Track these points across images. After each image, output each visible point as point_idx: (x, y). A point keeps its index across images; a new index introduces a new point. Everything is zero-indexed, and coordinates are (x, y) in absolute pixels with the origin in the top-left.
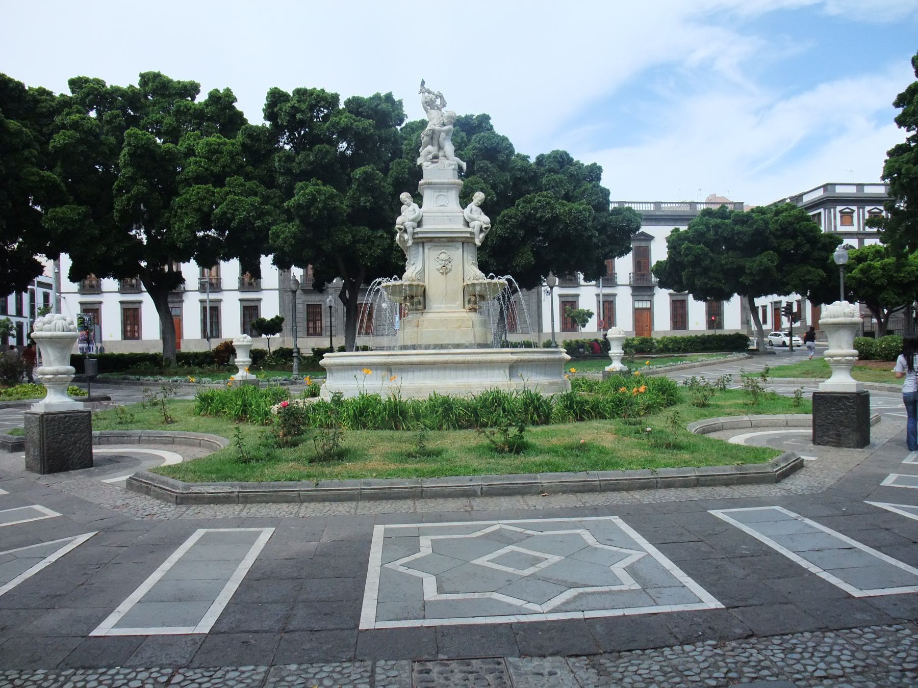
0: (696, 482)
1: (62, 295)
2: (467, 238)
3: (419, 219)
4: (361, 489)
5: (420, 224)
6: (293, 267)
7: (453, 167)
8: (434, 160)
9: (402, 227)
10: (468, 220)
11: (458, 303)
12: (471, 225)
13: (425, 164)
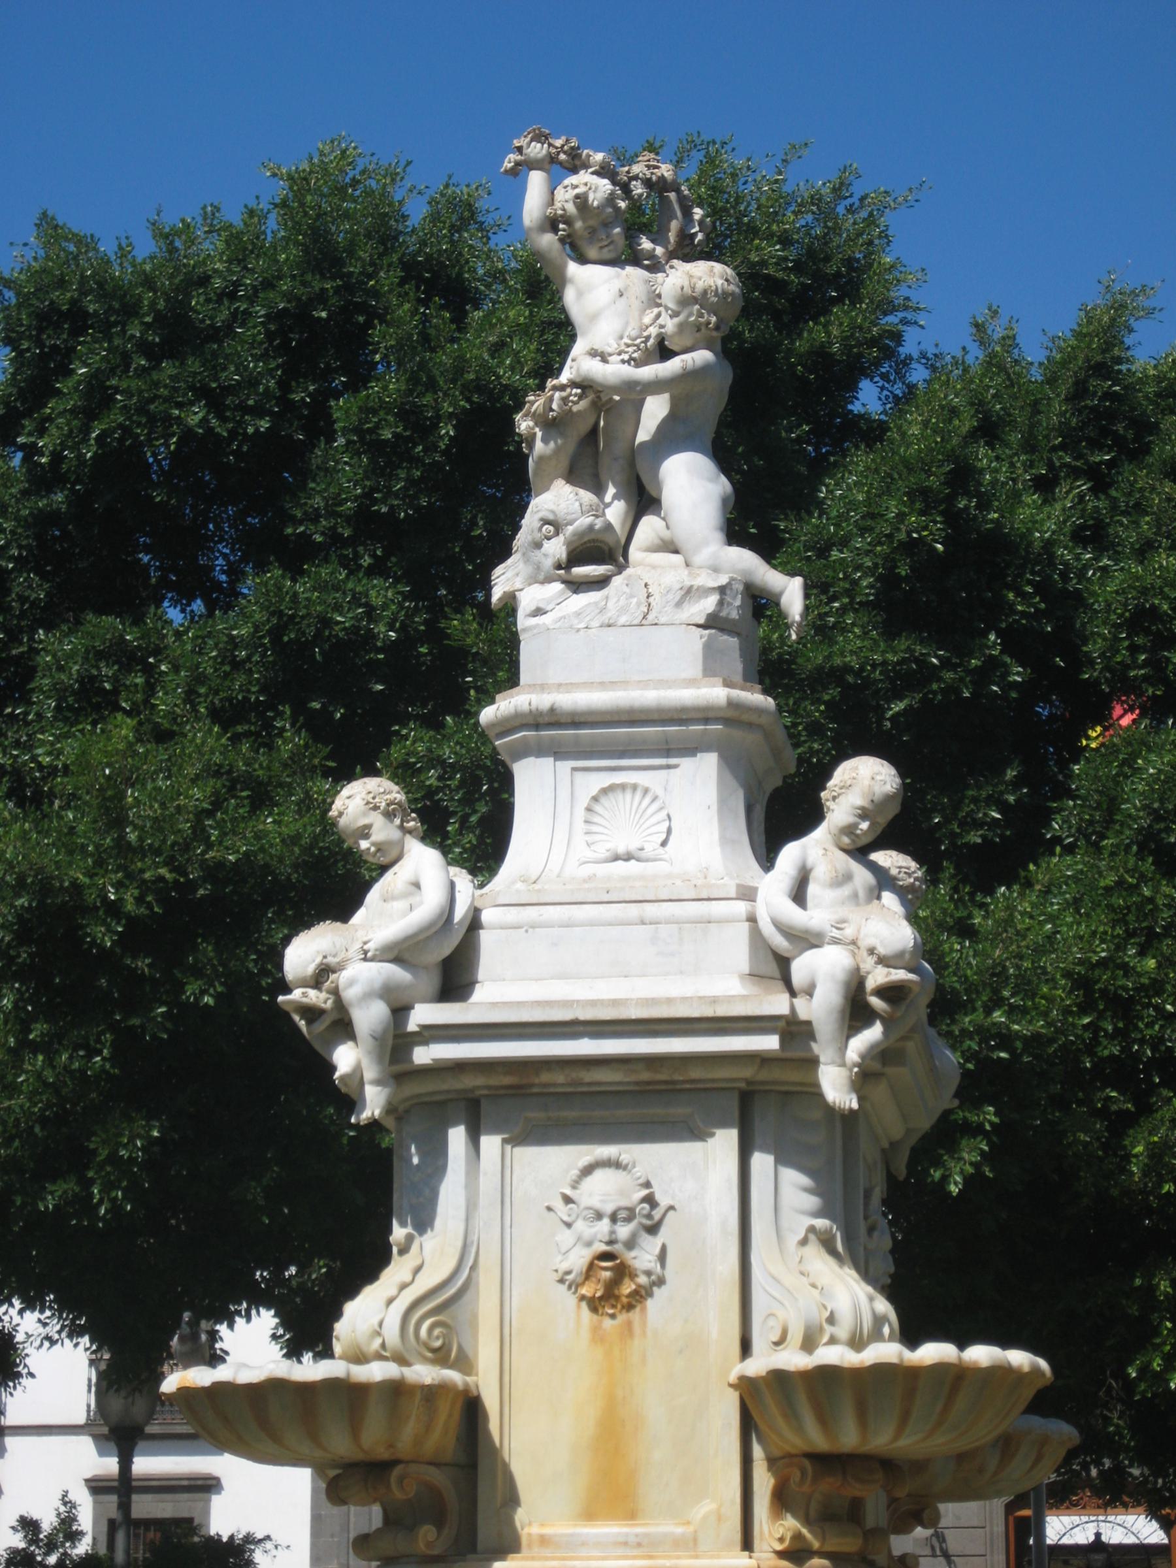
6: (1049, 1542)
7: (709, 604)
8: (580, 571)
9: (314, 997)
10: (779, 942)
11: (706, 1507)
12: (801, 968)
13: (528, 599)
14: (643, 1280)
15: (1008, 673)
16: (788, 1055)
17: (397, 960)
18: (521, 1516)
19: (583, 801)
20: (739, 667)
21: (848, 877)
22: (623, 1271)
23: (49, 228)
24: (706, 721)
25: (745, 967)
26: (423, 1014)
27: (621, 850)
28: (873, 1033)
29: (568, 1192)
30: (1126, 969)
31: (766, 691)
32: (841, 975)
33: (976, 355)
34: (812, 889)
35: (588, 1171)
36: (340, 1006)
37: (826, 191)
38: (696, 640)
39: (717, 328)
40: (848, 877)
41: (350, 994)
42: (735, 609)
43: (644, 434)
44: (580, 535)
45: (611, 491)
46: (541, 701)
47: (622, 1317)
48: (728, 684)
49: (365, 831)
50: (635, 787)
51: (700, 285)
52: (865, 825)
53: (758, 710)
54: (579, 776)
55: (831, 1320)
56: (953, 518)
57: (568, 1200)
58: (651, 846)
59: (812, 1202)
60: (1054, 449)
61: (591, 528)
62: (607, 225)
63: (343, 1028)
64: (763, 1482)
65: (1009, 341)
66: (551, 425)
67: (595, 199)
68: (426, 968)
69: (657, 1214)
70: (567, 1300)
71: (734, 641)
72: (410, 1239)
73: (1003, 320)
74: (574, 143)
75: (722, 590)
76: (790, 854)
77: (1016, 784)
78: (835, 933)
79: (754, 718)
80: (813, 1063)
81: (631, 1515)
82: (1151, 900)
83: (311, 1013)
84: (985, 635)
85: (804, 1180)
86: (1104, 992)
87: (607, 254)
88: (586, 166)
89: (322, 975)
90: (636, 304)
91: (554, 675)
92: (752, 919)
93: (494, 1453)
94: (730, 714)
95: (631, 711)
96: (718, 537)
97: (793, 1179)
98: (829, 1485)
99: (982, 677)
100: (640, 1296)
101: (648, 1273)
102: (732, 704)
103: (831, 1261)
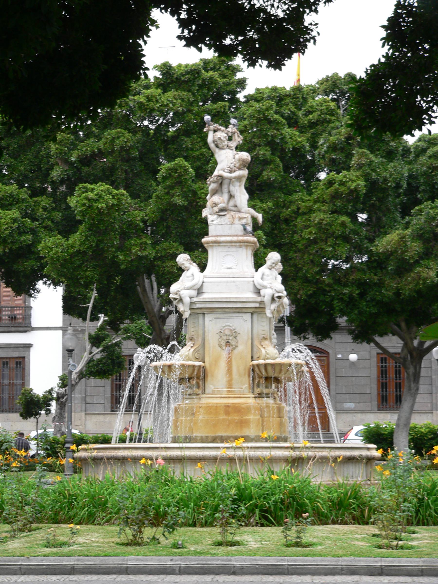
0: (380, 571)
2: (256, 308)
3: (198, 287)
4: (74, 564)
5: (200, 291)
9: (176, 296)
10: (259, 287)
12: (262, 292)
13: (210, 218)
41: (182, 296)
46: (213, 239)
58: (234, 267)
76: (260, 270)
92: (253, 282)
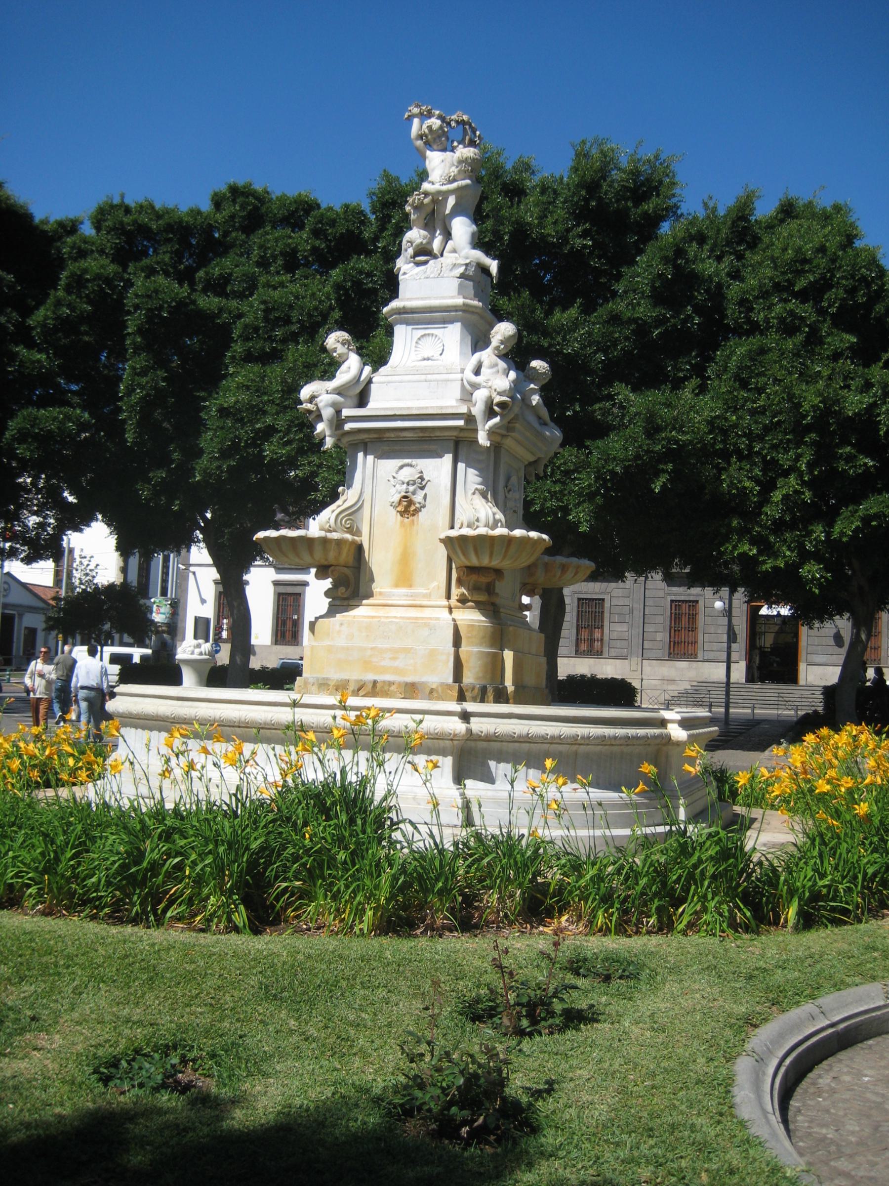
1: (192, 569)
7: (462, 270)
9: (309, 406)
11: (435, 584)
14: (418, 505)
15: (694, 319)
16: (469, 427)
17: (338, 394)
18: (374, 586)
19: (415, 339)
20: (473, 292)
21: (496, 365)
22: (411, 503)
23: (386, 175)
24: (456, 311)
25: (459, 398)
26: (346, 412)
27: (426, 357)
28: (497, 420)
29: (394, 475)
30: (726, 419)
31: (479, 301)
32: (484, 399)
33: (701, 214)
34: (483, 370)
35: (401, 467)
36: (318, 409)
37: (652, 158)
38: (457, 282)
39: (472, 171)
40: (496, 365)
41: (321, 405)
42: (471, 271)
43: (447, 212)
44: (418, 246)
45: (438, 232)
47: (411, 518)
48: (464, 298)
49: (335, 350)
50: (432, 335)
51: (465, 156)
52: (502, 347)
53: (476, 307)
54: (414, 331)
55: (478, 520)
56: (676, 267)
57: (394, 477)
58: (437, 356)
59: (479, 479)
60: (723, 246)
61: (422, 243)
62: (439, 137)
63: (319, 418)
64: (454, 575)
65: (714, 210)
66: (417, 208)
67: (435, 127)
68: (350, 397)
69: (424, 483)
70: (393, 512)
71: (471, 283)
72: (344, 491)
73: (714, 201)
74: (429, 107)
75: (467, 265)
77: (696, 356)
78: (485, 384)
79: (474, 310)
80: (476, 430)
81: (410, 586)
82: (736, 397)
83: (310, 412)
84: (686, 307)
85: (476, 472)
86: (718, 427)
87: (440, 147)
88: (433, 116)
89: (312, 399)
90: (448, 165)
91: (408, 295)
93: (366, 563)
94: (464, 308)
95: (430, 308)
96: (469, 246)
97: (472, 472)
98: (474, 577)
99: (685, 321)
100: (417, 511)
101: (420, 503)
102: (464, 305)
103: (483, 501)
